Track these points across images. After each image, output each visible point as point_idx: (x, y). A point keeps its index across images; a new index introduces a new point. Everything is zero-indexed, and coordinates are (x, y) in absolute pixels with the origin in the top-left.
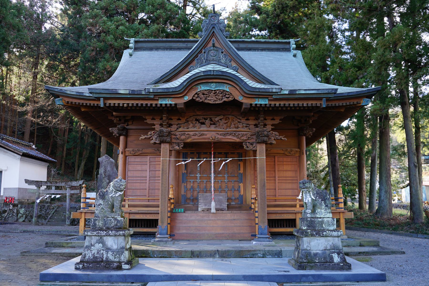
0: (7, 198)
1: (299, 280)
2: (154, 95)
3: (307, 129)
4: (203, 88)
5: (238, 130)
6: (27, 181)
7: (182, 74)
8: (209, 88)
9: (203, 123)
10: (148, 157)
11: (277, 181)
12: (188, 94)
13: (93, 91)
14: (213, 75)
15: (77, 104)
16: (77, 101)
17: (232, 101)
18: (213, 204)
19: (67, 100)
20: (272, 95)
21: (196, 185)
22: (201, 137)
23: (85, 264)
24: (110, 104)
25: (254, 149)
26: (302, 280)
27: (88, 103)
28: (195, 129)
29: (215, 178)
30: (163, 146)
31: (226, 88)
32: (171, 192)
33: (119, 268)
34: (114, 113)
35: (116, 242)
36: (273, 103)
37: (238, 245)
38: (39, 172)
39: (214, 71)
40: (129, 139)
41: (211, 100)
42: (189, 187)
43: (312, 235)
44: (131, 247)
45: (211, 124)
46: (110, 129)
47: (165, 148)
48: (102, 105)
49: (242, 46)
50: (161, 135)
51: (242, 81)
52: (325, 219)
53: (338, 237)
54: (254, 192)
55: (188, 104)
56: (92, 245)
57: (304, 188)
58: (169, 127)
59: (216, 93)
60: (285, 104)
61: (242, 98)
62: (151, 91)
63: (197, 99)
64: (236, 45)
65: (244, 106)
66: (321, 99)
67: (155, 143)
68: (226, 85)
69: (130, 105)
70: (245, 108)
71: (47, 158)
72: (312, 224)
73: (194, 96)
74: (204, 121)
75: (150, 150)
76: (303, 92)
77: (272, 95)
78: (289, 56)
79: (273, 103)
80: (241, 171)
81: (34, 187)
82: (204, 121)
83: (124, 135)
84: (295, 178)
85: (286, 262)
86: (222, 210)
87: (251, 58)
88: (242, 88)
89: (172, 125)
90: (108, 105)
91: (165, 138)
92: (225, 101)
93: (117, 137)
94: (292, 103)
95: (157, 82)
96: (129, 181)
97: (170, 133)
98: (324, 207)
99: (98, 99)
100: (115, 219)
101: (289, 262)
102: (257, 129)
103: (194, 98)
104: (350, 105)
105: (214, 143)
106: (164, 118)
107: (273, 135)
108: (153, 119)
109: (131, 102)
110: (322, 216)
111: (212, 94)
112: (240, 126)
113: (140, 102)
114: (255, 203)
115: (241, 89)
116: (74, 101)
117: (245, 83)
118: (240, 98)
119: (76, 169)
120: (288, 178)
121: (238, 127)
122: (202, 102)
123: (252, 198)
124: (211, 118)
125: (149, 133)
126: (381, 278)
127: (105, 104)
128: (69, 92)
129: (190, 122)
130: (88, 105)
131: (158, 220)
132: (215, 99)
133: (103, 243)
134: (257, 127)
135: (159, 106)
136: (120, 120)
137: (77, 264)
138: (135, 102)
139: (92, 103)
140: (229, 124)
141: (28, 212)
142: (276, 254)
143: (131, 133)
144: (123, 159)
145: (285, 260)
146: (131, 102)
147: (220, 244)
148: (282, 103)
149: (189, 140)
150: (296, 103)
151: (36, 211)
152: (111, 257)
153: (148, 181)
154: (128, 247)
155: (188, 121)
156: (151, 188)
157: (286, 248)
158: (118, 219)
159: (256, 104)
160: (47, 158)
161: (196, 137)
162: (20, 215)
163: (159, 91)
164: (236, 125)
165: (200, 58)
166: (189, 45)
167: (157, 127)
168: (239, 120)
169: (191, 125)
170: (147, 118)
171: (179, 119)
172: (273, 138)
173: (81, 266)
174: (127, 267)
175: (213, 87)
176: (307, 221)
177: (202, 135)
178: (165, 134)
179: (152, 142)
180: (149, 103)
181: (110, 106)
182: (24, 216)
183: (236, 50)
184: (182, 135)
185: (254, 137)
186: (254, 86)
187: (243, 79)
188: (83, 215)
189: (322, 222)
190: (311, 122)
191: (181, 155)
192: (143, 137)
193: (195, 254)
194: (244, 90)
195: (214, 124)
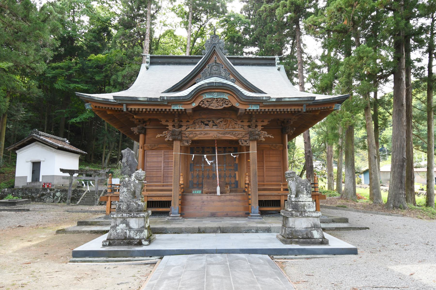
0: (45, 184)
1: (286, 253)
2: (168, 102)
3: (289, 129)
4: (207, 96)
5: (235, 130)
6: (62, 170)
7: (189, 85)
8: (211, 97)
9: (207, 125)
10: (163, 151)
11: (265, 170)
12: (196, 101)
13: (118, 98)
14: (216, 86)
15: (104, 108)
16: (104, 106)
17: (230, 107)
20: (263, 102)
21: (201, 173)
22: (206, 136)
23: (110, 242)
24: (131, 109)
25: (248, 145)
26: (289, 253)
27: (113, 107)
28: (201, 129)
31: (226, 97)
32: (181, 179)
33: (140, 244)
34: (135, 116)
35: (137, 222)
36: (263, 108)
37: (235, 222)
38: (72, 163)
39: (216, 83)
40: (147, 137)
41: (214, 106)
42: (195, 174)
43: (297, 216)
44: (149, 226)
45: (213, 125)
46: (132, 128)
47: (177, 145)
48: (125, 110)
49: (237, 61)
50: (173, 134)
51: (239, 91)
52: (307, 203)
53: (317, 217)
54: (247, 179)
55: (195, 110)
56: (117, 226)
57: (289, 178)
58: (180, 127)
59: (218, 100)
60: (272, 109)
61: (238, 104)
62: (166, 99)
63: (203, 106)
64: (232, 61)
65: (240, 111)
66: (302, 105)
67: (169, 140)
68: (225, 94)
69: (148, 110)
70: (241, 113)
71: (79, 150)
72: (296, 207)
73: (200, 103)
74: (208, 123)
75: (164, 146)
76: (288, 100)
77: (263, 102)
78: (274, 69)
79: (263, 108)
81: (68, 175)
82: (208, 123)
83: (143, 133)
84: (280, 168)
85: (275, 237)
87: (245, 72)
88: (238, 96)
89: (182, 126)
90: (129, 110)
91: (177, 137)
92: (225, 107)
93: (137, 135)
94: (278, 109)
95: (169, 91)
96: (147, 170)
97: (180, 133)
98: (305, 192)
99: (122, 105)
100: (136, 204)
101: (277, 237)
102: (250, 129)
103: (200, 105)
104: (324, 109)
105: (217, 140)
106: (176, 121)
107: (263, 134)
108: (167, 121)
109: (148, 108)
110: (304, 200)
111: (214, 101)
112: (236, 127)
113: (156, 108)
114: (248, 187)
115: (237, 97)
116: (101, 106)
117: (241, 92)
118: (237, 105)
119: (103, 159)
120: (273, 168)
121: (234, 128)
122: (207, 107)
123: (245, 184)
124: (213, 121)
125: (164, 132)
126: (354, 252)
127: (127, 109)
128: (96, 99)
129: (196, 124)
130: (113, 109)
131: (170, 201)
132: (217, 105)
133: (128, 225)
134: (250, 128)
135: (171, 111)
136: (139, 121)
137: (105, 241)
138: (152, 108)
139: (116, 107)
140: (227, 125)
141: (62, 195)
142: (266, 230)
143: (148, 131)
144: (142, 153)
145: (273, 236)
146: (148, 108)
147: (221, 221)
148: (271, 108)
149: (196, 138)
150: (282, 108)
151: (70, 194)
152: (132, 234)
153: (162, 170)
154: (147, 226)
155: (195, 123)
156: (165, 176)
157: (274, 225)
158: (139, 203)
159: (250, 110)
160: (79, 150)
161: (202, 136)
162: (56, 197)
163: (172, 99)
164: (233, 126)
165: (205, 72)
166: (195, 61)
167: (170, 128)
168: (236, 122)
169: (198, 126)
170: (162, 120)
171: (188, 121)
172: (263, 136)
173: (108, 243)
174: (146, 243)
175: (215, 95)
176: (292, 204)
177: (206, 134)
178: (176, 133)
179: (166, 139)
180: (164, 108)
181: (131, 111)
182: (59, 198)
183: (232, 65)
184: (190, 134)
185: (248, 136)
186: (248, 95)
187: (239, 89)
188: (109, 198)
189: (304, 205)
190: (292, 123)
191: (189, 150)
192: (159, 136)
193: (201, 230)
194: (240, 98)
195: (216, 125)
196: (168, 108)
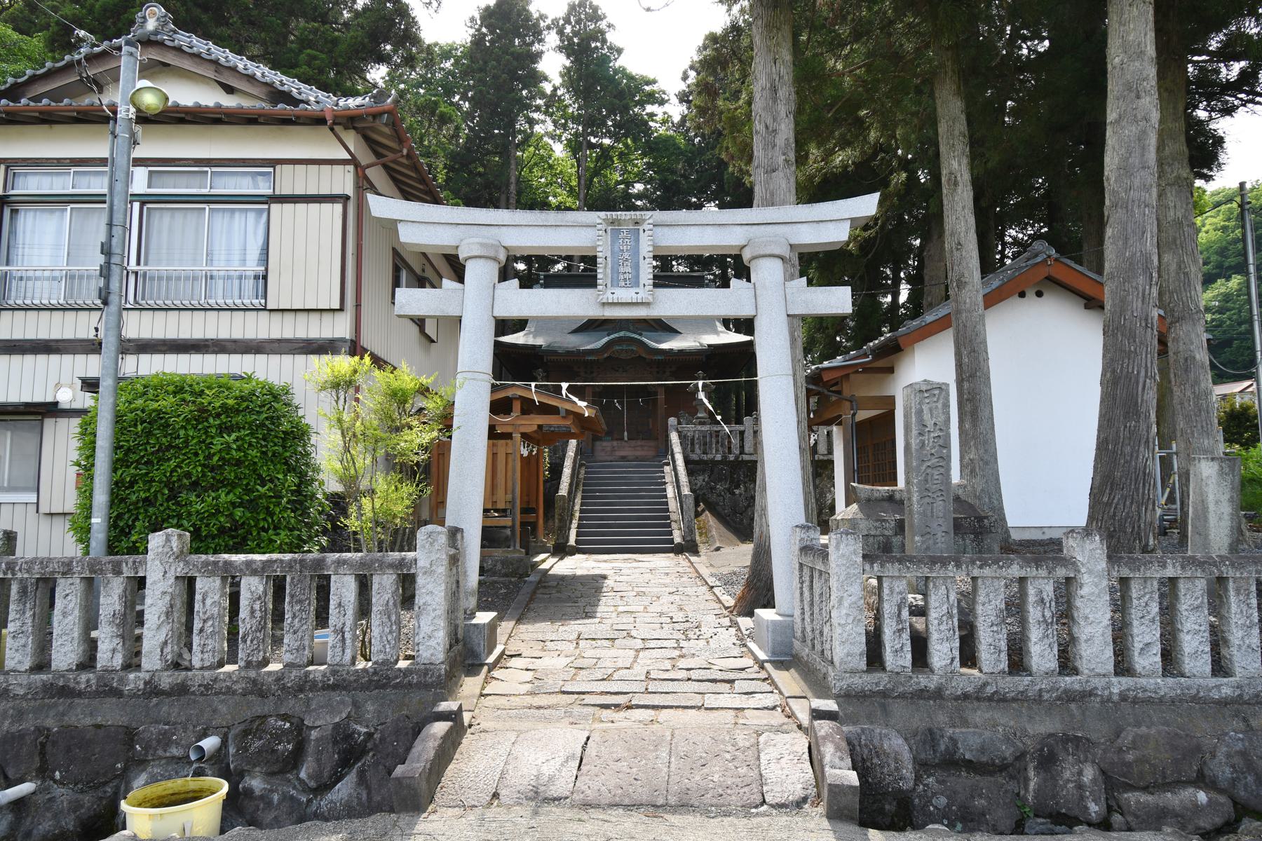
41: (623, 356)
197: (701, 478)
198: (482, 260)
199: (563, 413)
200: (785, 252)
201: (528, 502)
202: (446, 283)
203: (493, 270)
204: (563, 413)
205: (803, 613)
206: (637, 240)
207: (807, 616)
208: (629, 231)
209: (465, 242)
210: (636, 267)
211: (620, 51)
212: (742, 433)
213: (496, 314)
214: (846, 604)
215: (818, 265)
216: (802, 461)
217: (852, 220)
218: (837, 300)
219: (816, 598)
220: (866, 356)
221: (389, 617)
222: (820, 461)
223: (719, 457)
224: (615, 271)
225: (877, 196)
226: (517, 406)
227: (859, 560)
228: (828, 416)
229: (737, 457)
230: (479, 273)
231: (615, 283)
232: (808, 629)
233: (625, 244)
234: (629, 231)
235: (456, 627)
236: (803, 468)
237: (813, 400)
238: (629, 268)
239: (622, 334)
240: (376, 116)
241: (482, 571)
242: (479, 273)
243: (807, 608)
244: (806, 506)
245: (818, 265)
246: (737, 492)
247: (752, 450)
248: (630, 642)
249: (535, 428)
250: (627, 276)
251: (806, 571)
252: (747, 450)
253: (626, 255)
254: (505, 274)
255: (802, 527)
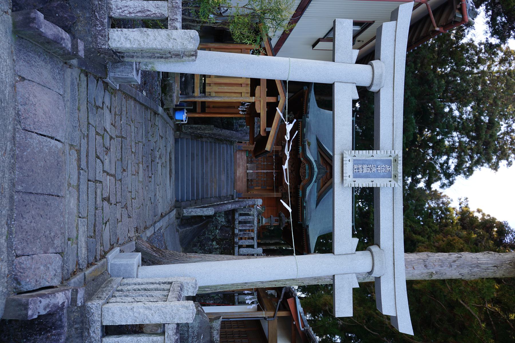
4: (307, 167)
18: (251, 171)
19: (306, 92)
29: (264, 172)
30: (281, 147)
41: (301, 170)
80: (268, 188)
86: (247, 176)
118: (302, 184)
196: (300, 144)
197: (224, 220)
198: (371, 76)
199: (268, 129)
200: (375, 274)
201: (209, 107)
202: (356, 52)
203: (365, 82)
204: (268, 129)
205: (139, 284)
206: (383, 177)
207: (136, 287)
208: (390, 172)
209: (383, 64)
210: (366, 176)
211: (510, 164)
212: (252, 246)
213: (336, 84)
214: (147, 312)
215: (367, 293)
216: (237, 285)
217: (396, 318)
218: (344, 307)
219: (149, 293)
220: (304, 326)
221: (140, 11)
222: (234, 296)
223: (236, 231)
224: (364, 162)
225: (412, 333)
226: (272, 100)
227: (177, 321)
228: (265, 301)
229: (237, 243)
230: (363, 74)
231: (356, 162)
232: (129, 287)
233: (382, 169)
234: (390, 172)
235: (133, 57)
236: (233, 285)
237: (273, 292)
238: (365, 170)
239: (316, 170)
240: (461, 10)
241: (166, 75)
242: (363, 74)
243: (143, 287)
244: (208, 287)
245: (367, 293)
246: (214, 243)
247: (241, 253)
248: (119, 170)
249: (258, 111)
250: (361, 170)
251: (167, 287)
252: (241, 249)
253: (374, 169)
254: (363, 91)
255: (196, 284)
